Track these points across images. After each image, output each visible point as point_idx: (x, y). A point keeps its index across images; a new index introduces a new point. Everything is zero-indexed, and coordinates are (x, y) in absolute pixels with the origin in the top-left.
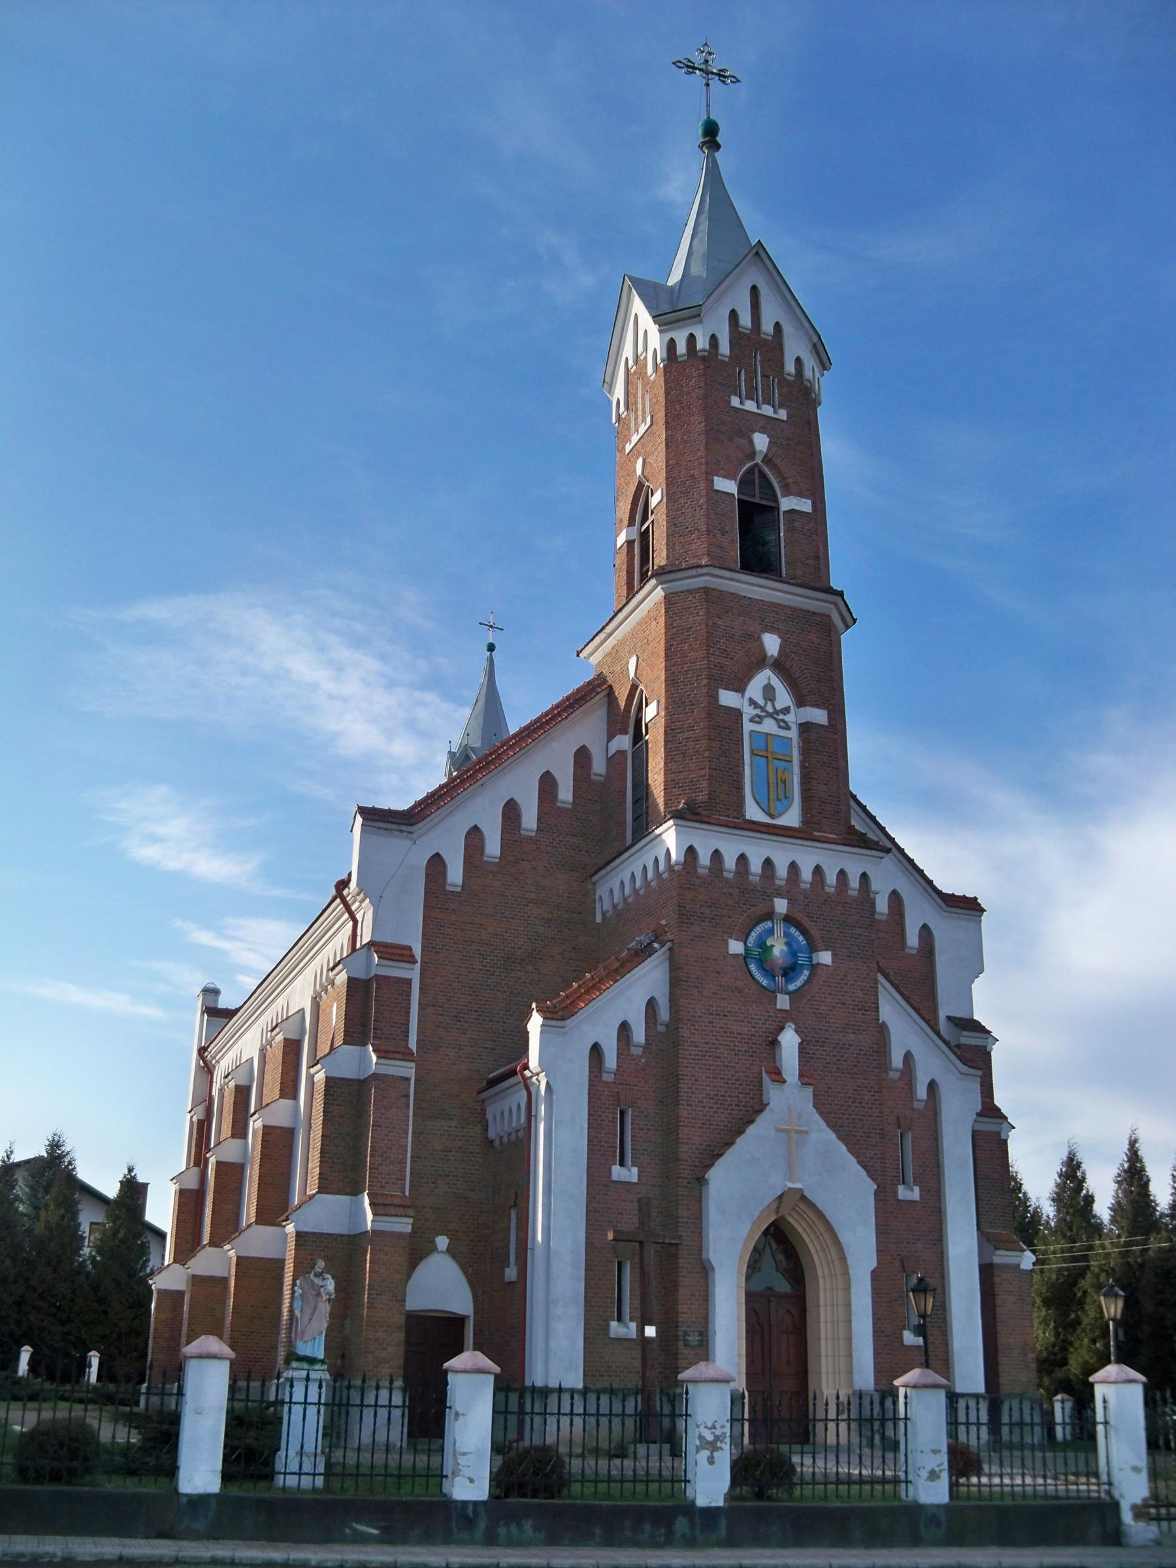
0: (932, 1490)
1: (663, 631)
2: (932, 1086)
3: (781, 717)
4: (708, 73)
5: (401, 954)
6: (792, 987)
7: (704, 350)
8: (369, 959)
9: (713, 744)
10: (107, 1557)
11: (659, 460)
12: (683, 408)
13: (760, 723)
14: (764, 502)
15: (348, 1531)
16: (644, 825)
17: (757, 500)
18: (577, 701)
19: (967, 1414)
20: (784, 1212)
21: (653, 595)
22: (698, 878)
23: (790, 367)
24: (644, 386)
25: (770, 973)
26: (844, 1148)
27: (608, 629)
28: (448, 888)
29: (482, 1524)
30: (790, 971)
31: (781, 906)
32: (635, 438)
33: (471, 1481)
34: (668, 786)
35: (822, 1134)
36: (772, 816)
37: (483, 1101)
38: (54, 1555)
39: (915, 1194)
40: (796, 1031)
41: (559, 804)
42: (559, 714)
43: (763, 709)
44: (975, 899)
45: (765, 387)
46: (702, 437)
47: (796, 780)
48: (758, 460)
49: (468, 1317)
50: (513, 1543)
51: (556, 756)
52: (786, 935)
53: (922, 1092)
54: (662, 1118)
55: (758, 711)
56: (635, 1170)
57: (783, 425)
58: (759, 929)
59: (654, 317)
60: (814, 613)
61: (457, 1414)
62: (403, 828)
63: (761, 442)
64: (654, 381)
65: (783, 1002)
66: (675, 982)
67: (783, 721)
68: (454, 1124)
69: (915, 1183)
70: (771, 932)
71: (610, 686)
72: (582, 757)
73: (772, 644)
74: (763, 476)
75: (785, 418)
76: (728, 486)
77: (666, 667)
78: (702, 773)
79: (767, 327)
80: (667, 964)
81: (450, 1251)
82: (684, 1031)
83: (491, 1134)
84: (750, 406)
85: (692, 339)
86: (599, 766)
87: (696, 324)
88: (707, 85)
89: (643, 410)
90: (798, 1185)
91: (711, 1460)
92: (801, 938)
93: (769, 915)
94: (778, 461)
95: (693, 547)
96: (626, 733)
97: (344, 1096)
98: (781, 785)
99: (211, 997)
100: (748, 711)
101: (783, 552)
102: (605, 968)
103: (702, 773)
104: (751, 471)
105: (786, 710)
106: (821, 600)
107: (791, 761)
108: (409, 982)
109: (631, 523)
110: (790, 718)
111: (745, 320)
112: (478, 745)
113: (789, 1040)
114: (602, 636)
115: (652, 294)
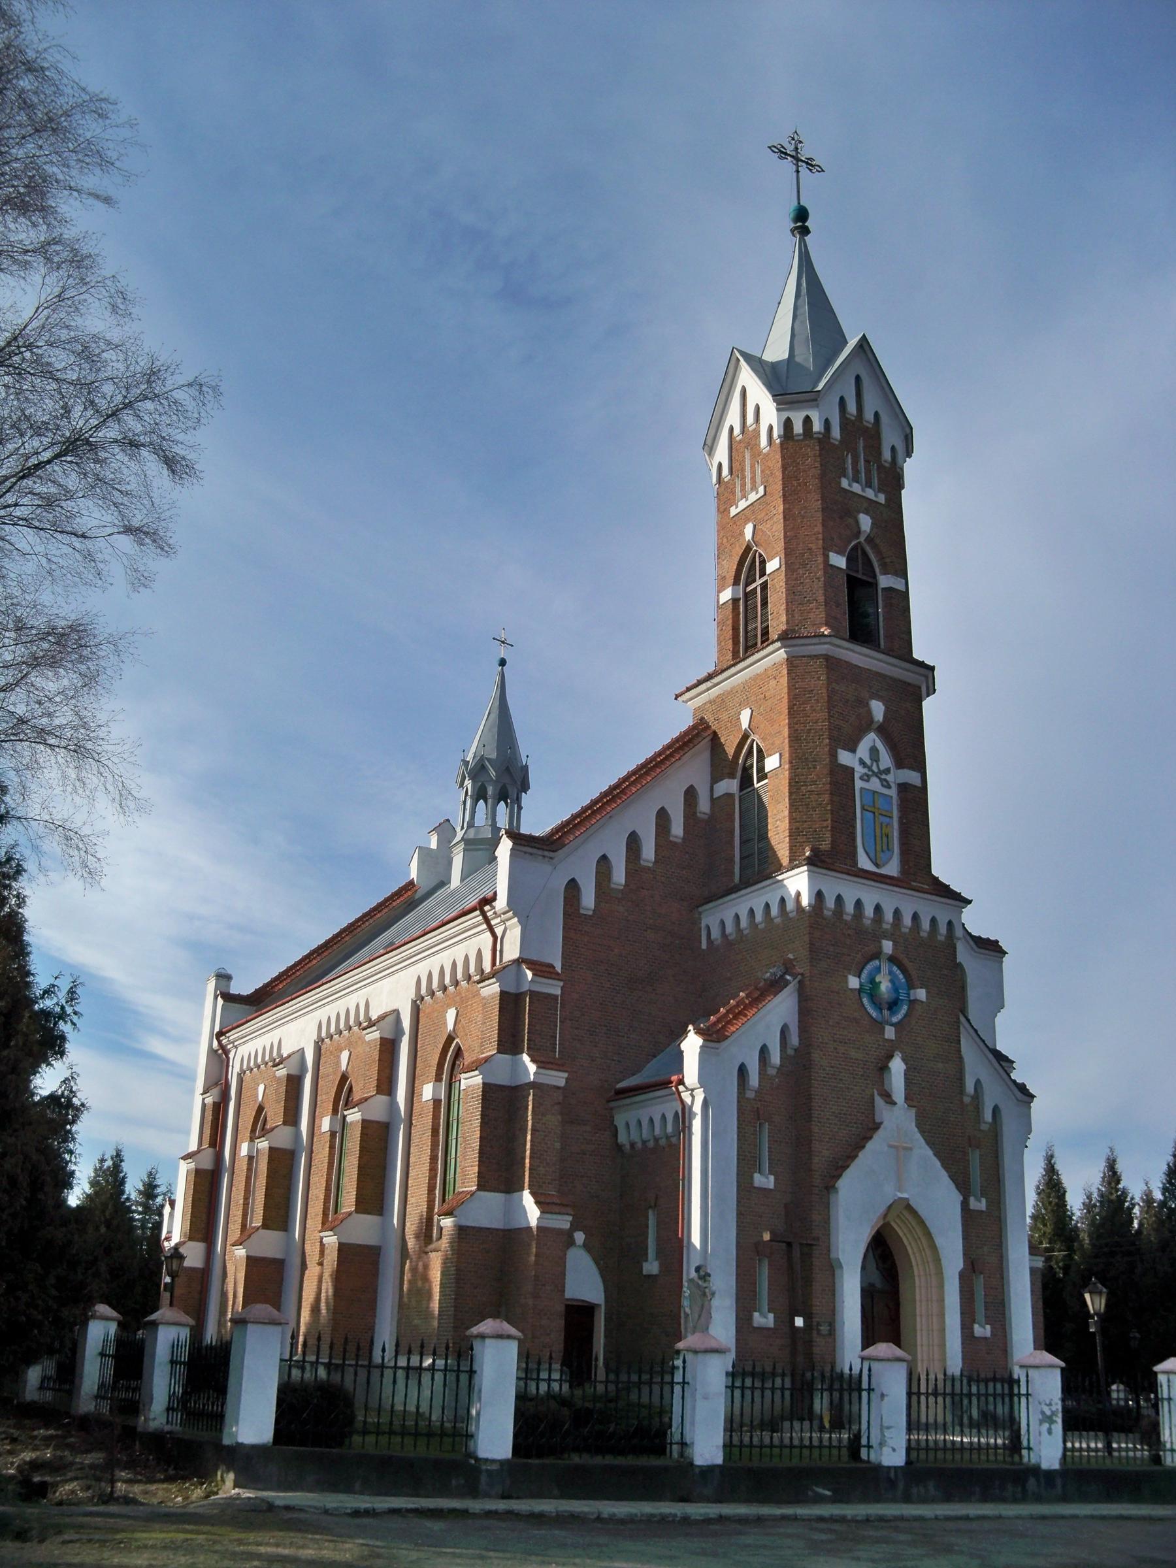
0: (892, 1453)
1: (786, 690)
2: (996, 1111)
3: (884, 776)
4: (798, 160)
5: (542, 970)
6: (895, 1020)
7: (819, 433)
8: (520, 975)
10: (712, 1516)
11: (776, 528)
12: (799, 485)
14: (864, 578)
15: (810, 1493)
16: (761, 867)
17: (860, 576)
18: (685, 744)
19: (953, 1386)
20: (890, 1218)
21: (774, 656)
24: (753, 456)
25: (878, 1006)
26: (938, 1164)
27: (716, 680)
28: (582, 911)
29: (901, 1485)
30: (893, 1005)
32: (743, 504)
33: (894, 1450)
34: (794, 833)
35: (923, 1151)
36: (877, 865)
37: (612, 1109)
38: (676, 1515)
40: (903, 1060)
42: (671, 755)
43: (870, 768)
44: (997, 942)
45: (868, 472)
46: (820, 514)
47: (896, 834)
48: (862, 539)
49: (599, 1306)
50: (924, 1500)
51: (669, 794)
52: (890, 973)
53: (988, 1116)
54: (797, 1133)
55: (865, 770)
56: (772, 1178)
58: (869, 967)
59: (773, 396)
60: (909, 684)
61: (883, 1396)
62: (546, 853)
63: (865, 522)
64: (767, 454)
65: (890, 1033)
66: (805, 1011)
68: (588, 1128)
69: (771, 1173)
70: (878, 970)
71: (715, 733)
72: (690, 795)
73: (878, 709)
74: (864, 553)
75: (883, 502)
76: (840, 561)
77: (789, 724)
78: (825, 824)
79: (869, 416)
80: (796, 994)
81: (586, 1246)
82: (816, 1055)
83: (622, 1138)
85: (807, 421)
86: (704, 806)
87: (812, 407)
88: (798, 172)
89: (753, 479)
90: (905, 1195)
91: (1050, 1432)
92: (901, 976)
93: (877, 955)
94: (878, 541)
95: (812, 615)
96: (734, 778)
97: (501, 1103)
98: (885, 839)
99: (223, 982)
100: (859, 770)
101: (881, 624)
103: (825, 824)
104: (855, 548)
105: (887, 771)
106: (908, 670)
107: (891, 817)
109: (736, 582)
110: (890, 778)
111: (852, 408)
112: (494, 756)
113: (897, 1066)
114: (709, 684)
115: (758, 365)
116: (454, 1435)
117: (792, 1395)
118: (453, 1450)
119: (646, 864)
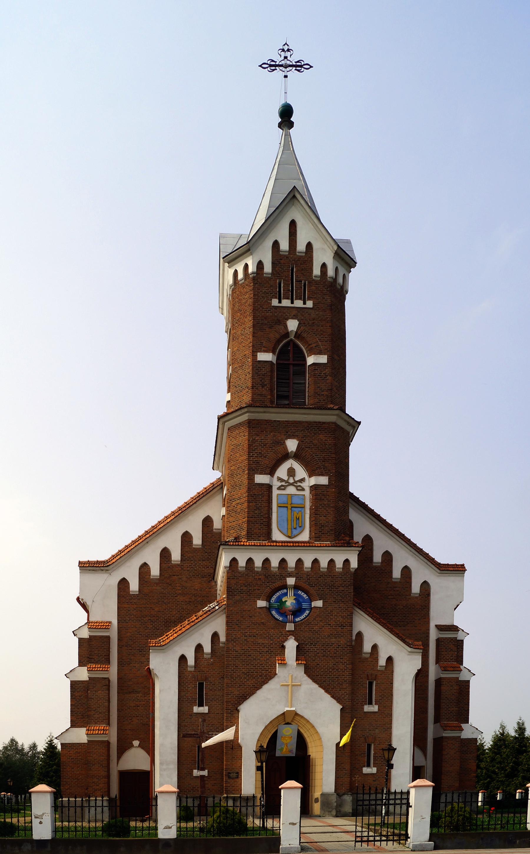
3: (299, 484)
9: (251, 504)
13: (284, 489)
22: (239, 573)
23: (317, 271)
31: (291, 581)
39: (375, 708)
41: (194, 546)
57: (311, 311)
58: (278, 594)
63: (292, 325)
67: (300, 486)
70: (286, 594)
73: (292, 445)
79: (301, 247)
84: (286, 303)
90: (293, 709)
92: (305, 596)
93: (285, 586)
100: (276, 484)
102: (188, 621)
105: (302, 480)
107: (304, 507)
108: (108, 638)
111: (284, 246)
116: (25, 830)
117: (116, 804)
118: (19, 836)
119: (377, 565)
